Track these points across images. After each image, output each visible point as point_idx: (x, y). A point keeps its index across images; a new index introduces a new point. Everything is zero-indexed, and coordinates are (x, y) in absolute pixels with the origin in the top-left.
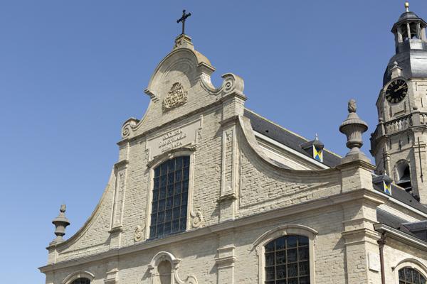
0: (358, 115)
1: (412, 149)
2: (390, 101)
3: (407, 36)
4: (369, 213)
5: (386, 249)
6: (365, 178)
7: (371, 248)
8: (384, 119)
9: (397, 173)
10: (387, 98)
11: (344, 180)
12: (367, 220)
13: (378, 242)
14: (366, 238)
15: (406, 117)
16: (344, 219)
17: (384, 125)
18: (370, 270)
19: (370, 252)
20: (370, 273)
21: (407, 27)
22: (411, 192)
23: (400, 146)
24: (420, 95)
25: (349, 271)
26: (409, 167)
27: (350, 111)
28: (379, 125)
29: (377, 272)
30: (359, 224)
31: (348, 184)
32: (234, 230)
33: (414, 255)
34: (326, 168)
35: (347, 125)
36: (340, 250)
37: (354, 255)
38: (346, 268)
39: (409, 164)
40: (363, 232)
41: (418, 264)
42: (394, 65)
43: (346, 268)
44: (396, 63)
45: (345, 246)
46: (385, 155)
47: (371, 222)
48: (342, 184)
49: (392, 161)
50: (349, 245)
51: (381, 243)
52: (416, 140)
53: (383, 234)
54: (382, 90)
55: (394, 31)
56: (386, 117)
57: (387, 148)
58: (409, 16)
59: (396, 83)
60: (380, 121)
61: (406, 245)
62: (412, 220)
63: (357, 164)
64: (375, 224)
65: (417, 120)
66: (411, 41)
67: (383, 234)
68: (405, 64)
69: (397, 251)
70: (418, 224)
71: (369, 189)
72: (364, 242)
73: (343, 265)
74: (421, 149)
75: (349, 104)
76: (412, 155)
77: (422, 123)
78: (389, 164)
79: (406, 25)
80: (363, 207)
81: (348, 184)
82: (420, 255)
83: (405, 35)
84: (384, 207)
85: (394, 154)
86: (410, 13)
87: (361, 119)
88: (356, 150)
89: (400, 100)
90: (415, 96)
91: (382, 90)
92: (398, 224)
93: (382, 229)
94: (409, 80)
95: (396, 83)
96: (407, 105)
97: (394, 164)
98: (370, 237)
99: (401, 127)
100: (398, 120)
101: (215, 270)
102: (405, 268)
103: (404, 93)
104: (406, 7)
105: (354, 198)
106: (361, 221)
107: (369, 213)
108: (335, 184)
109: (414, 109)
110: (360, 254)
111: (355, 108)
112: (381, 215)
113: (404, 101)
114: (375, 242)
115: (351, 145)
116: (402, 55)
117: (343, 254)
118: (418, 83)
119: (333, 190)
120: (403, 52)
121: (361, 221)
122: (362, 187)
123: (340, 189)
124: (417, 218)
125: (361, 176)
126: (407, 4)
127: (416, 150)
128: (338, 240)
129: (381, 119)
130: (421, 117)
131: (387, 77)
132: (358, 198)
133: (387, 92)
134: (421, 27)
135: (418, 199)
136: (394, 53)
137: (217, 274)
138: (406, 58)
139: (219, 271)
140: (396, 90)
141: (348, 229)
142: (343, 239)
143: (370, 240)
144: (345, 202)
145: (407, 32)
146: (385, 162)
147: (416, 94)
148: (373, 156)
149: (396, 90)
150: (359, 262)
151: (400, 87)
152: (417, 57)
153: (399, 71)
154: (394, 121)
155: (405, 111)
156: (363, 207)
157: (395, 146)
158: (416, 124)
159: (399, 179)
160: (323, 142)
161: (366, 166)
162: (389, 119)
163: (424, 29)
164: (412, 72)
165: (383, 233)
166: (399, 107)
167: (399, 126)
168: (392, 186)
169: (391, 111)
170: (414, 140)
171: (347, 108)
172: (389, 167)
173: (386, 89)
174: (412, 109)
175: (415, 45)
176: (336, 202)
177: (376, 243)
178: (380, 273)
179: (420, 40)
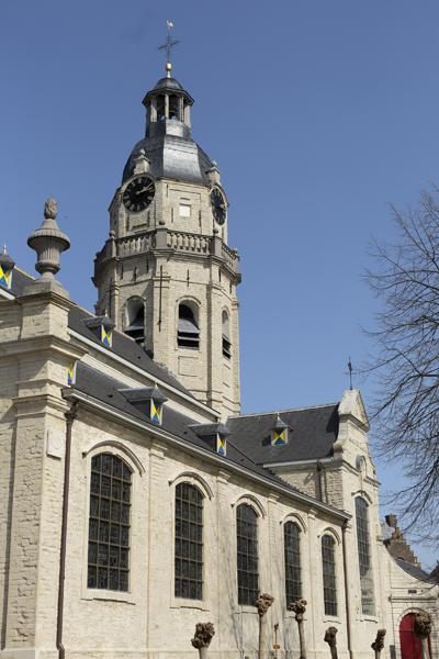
0: (58, 224)
1: (151, 282)
2: (128, 208)
3: (164, 114)
4: (58, 374)
5: (78, 425)
6: (56, 321)
7: (53, 426)
8: (117, 233)
9: (127, 316)
10: (125, 201)
11: (26, 319)
12: (52, 382)
13: (66, 415)
14: (48, 409)
15: (148, 234)
16: (19, 378)
17: (116, 243)
18: (49, 456)
19: (52, 429)
20: (47, 461)
21: (167, 99)
22: (143, 344)
23: (135, 276)
24: (172, 204)
25: (17, 456)
26: (143, 308)
27: (47, 216)
28: (109, 242)
29: (59, 459)
30: (41, 388)
31: (30, 327)
32: (210, 464)
33: (119, 436)
34: (12, 298)
35: (42, 236)
36: (8, 425)
37: (28, 433)
38: (13, 452)
39: (145, 304)
40: (44, 400)
41: (125, 452)
42: (140, 154)
43: (13, 452)
44: (143, 151)
45: (16, 419)
46: (112, 287)
47: (58, 385)
48: (21, 326)
49: (121, 297)
50: (22, 417)
51: (70, 417)
52: (158, 270)
53: (75, 404)
54: (119, 189)
55: (147, 102)
56: (120, 231)
57: (117, 278)
58: (169, 84)
59: (140, 182)
60: (111, 235)
61: (106, 421)
62: (134, 385)
63: (46, 297)
64: (64, 389)
65: (164, 241)
66: (168, 121)
67: (75, 404)
68: (156, 156)
69: (93, 430)
70: (142, 391)
71: (60, 336)
72: (43, 415)
73: (9, 447)
74: (164, 284)
75: (47, 205)
76: (150, 291)
77: (169, 246)
78: (117, 301)
79: (164, 97)
80: (49, 362)
81: (30, 327)
82: (126, 436)
83: (161, 112)
84: (89, 360)
85: (125, 288)
86: (172, 80)
87: (61, 231)
88: (48, 276)
89: (143, 208)
90: (164, 205)
91: (119, 189)
92: (109, 391)
93: (74, 397)
94: (159, 179)
95: (140, 182)
96: (152, 216)
97: (124, 301)
98: (54, 407)
99: (139, 248)
100: (136, 237)
101: (12, 417)
102: (104, 454)
103: (149, 198)
104: (168, 70)
105: (37, 348)
106: (42, 383)
107: (58, 374)
108: (11, 324)
109: (161, 223)
110: (36, 432)
111: (54, 212)
112: (85, 375)
113: (147, 210)
114: (61, 415)
115: (41, 268)
116: (154, 141)
117: (11, 431)
118: (171, 187)
119: (8, 334)
120: (155, 137)
121: (42, 383)
122: (51, 333)
123: (18, 333)
124: (143, 383)
125: (51, 316)
126: (169, 66)
127: (157, 284)
128: (6, 410)
129: (113, 232)
130: (169, 236)
131: (128, 172)
132: (43, 348)
133: (126, 193)
134: (186, 103)
135: (151, 355)
136: (144, 137)
137: (14, 427)
138: (159, 146)
139: (20, 422)
140: (138, 193)
141: (23, 393)
142: (15, 408)
143: (54, 411)
144: (25, 353)
145: (164, 108)
146: (111, 298)
147: (166, 201)
148: (96, 285)
149: (138, 193)
150: (33, 443)
151: (145, 189)
152: (174, 147)
153: (146, 164)
154: (131, 238)
155: (147, 225)
156: (49, 362)
157: (128, 276)
158: (160, 245)
159: (128, 324)
160: (14, 259)
161: (59, 301)
162: (124, 233)
163: (188, 107)
164: (165, 168)
165: (75, 402)
166: (139, 218)
167: (138, 246)
168: (116, 335)
169: (128, 223)
170: (155, 268)
171: (42, 212)
172: (116, 306)
173: (124, 188)
174: (157, 223)
175: (174, 129)
176: (10, 352)
177: (63, 417)
178: (63, 460)
179: (181, 123)
